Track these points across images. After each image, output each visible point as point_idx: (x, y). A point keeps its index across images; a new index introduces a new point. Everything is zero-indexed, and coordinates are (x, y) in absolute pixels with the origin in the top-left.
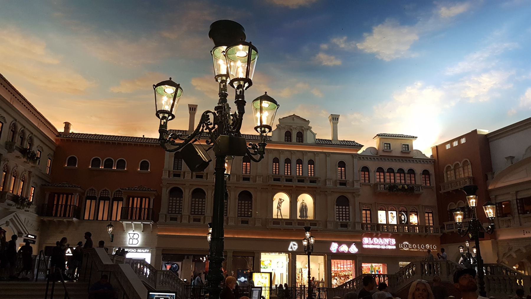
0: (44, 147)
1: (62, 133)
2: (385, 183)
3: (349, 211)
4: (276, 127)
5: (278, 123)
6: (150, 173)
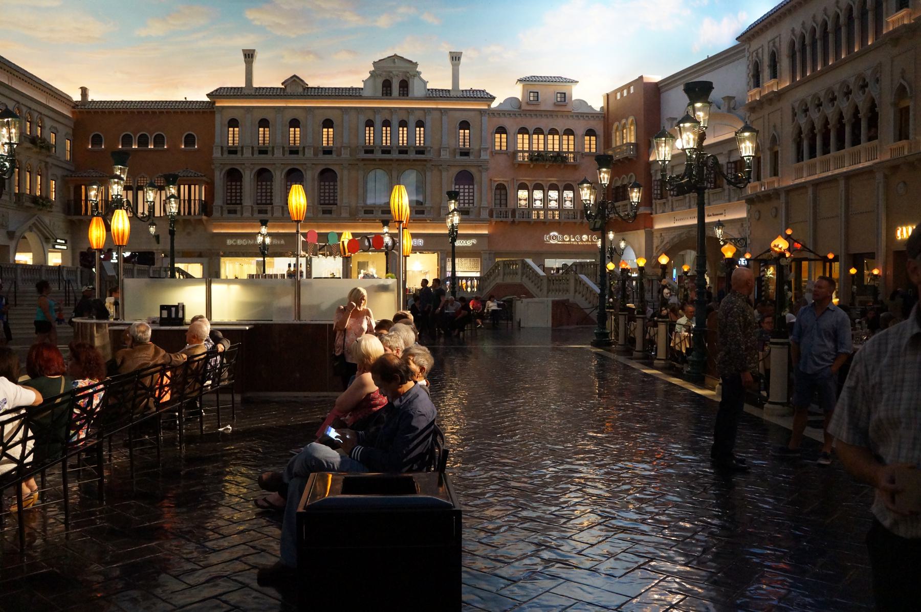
1: (79, 101)
2: (530, 151)
5: (373, 69)
6: (198, 150)
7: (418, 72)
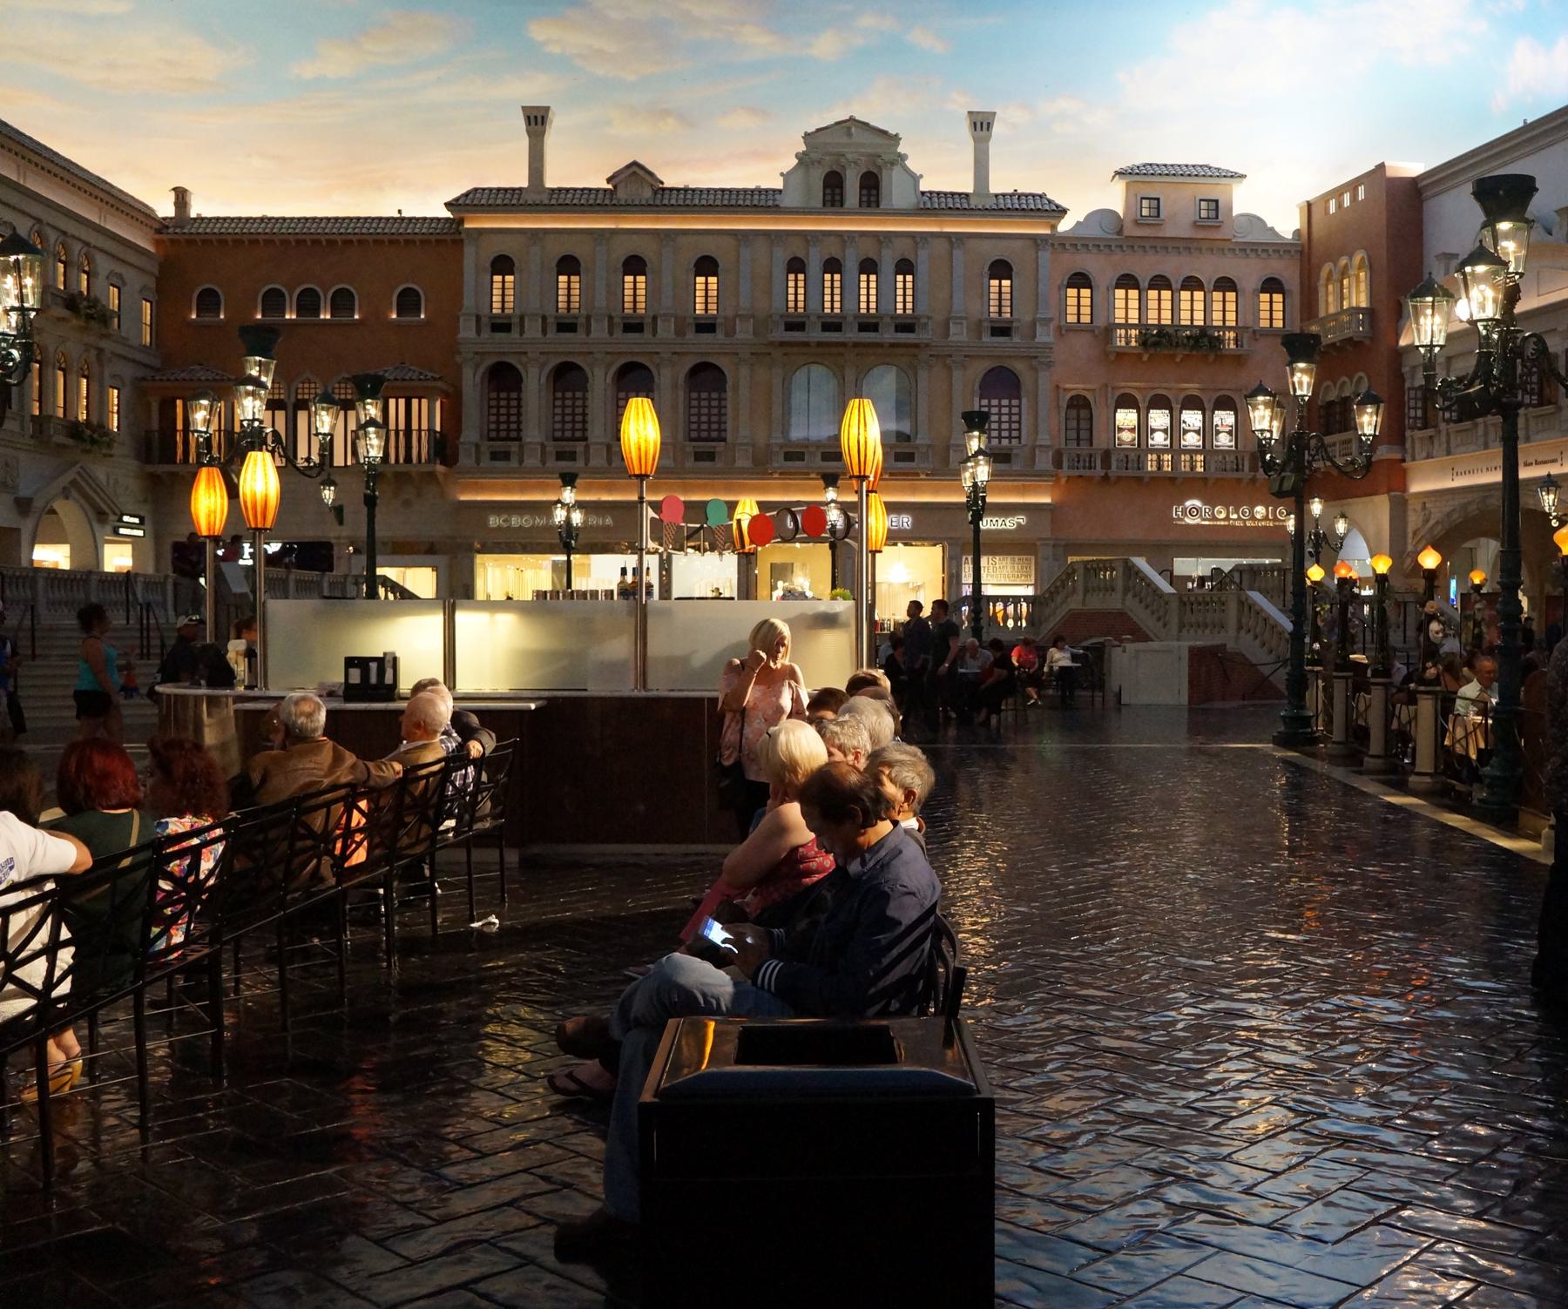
0: (128, 274)
1: (171, 218)
2: (1142, 326)
3: (1019, 414)
4: (796, 161)
6: (427, 322)
7: (900, 155)
